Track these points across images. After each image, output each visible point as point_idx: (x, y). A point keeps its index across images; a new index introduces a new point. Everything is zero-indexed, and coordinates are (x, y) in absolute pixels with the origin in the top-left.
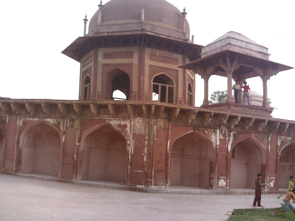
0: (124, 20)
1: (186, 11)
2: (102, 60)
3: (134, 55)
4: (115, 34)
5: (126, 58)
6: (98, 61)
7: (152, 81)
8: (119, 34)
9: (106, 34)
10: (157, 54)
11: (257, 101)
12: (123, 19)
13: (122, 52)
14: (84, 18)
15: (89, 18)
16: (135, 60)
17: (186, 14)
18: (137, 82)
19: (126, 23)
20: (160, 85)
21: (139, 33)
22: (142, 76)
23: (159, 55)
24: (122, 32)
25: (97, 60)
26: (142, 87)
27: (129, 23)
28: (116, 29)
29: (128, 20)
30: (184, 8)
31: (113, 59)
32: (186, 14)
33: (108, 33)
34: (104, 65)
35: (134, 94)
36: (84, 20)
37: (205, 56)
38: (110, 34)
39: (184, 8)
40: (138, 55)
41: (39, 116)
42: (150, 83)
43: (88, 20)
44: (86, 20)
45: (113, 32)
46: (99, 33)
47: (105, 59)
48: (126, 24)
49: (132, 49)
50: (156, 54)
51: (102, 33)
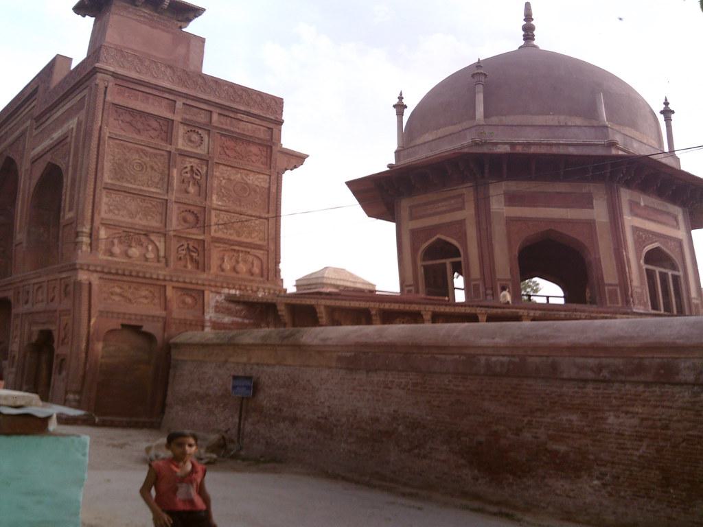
0: (552, 117)
1: (671, 107)
2: (505, 208)
3: (594, 201)
4: (533, 150)
5: (572, 207)
6: (491, 210)
7: (642, 262)
8: (543, 150)
9: (507, 149)
10: (642, 204)
11: (96, 175)
12: (549, 114)
13: (561, 193)
14: (396, 101)
15: (412, 103)
16: (599, 212)
17: (673, 112)
18: (614, 263)
19: (557, 124)
20: (658, 270)
21: (601, 152)
22: (624, 250)
23: (645, 206)
24: (551, 145)
25: (490, 209)
26: (628, 274)
27: (566, 126)
28: (533, 136)
29: (562, 118)
30: (666, 100)
31: (534, 206)
32: (673, 112)
33: (513, 145)
34: (510, 221)
35: (611, 288)
36: (395, 106)
37: (95, 139)
38: (519, 149)
39: (666, 100)
40: (605, 203)
41: (631, 409)
42: (640, 267)
43: (406, 107)
44: (400, 107)
45: (529, 144)
46: (486, 143)
47: (509, 206)
48: (557, 126)
49: (588, 188)
50: (640, 204)
51: (496, 144)
